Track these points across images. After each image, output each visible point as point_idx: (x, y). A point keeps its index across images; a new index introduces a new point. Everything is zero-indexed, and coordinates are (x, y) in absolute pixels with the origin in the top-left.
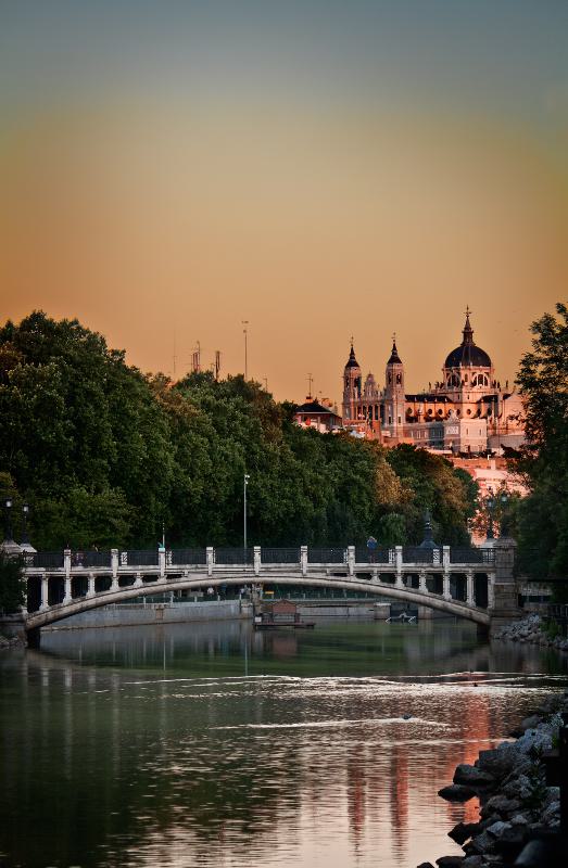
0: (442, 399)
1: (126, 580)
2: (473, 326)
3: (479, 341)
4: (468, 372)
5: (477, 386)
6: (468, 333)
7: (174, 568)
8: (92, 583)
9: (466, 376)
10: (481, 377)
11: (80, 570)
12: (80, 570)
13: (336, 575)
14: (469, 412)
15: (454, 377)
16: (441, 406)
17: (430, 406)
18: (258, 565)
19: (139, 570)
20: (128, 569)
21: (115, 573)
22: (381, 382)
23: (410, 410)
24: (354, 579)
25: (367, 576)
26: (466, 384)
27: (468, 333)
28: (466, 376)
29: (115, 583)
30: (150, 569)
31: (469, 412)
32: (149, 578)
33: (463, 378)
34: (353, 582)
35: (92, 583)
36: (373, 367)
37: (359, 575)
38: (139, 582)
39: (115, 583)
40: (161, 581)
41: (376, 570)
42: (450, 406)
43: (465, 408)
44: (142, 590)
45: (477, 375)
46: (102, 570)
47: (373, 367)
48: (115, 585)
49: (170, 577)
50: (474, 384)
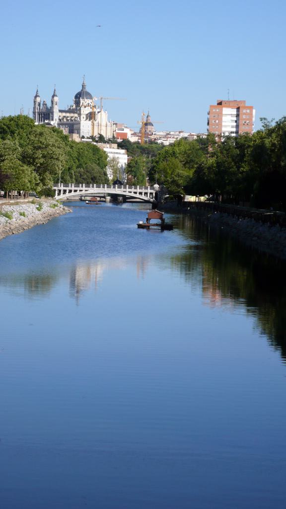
1: (75, 191)
3: (88, 89)
5: (87, 108)
6: (83, 86)
11: (65, 188)
12: (65, 188)
17: (68, 115)
18: (106, 188)
20: (76, 189)
23: (60, 116)
35: (73, 191)
37: (129, 192)
38: (78, 191)
45: (87, 103)
46: (146, 191)
49: (86, 191)
50: (85, 107)
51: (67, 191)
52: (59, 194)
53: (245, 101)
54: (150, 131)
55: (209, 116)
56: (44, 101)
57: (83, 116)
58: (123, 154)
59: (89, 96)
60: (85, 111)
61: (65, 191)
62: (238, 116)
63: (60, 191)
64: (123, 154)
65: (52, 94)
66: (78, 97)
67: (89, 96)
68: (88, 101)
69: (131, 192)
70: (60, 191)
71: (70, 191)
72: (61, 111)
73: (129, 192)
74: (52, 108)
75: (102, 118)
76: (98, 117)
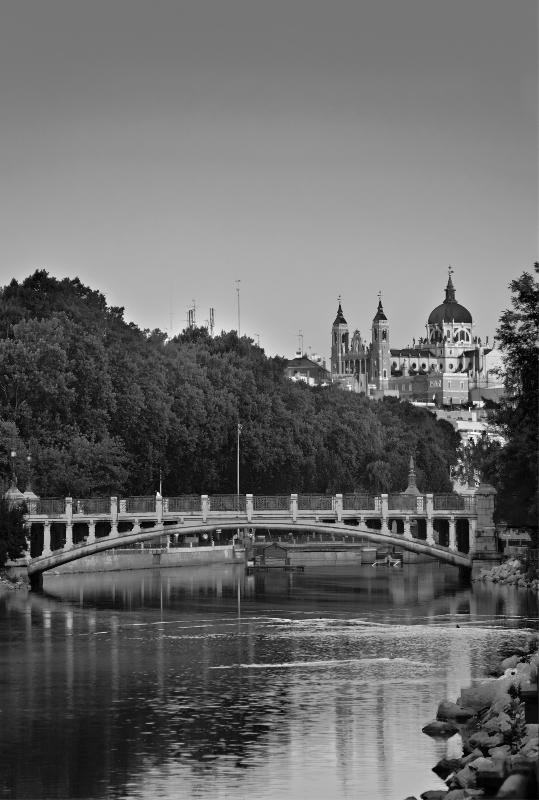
0: (426, 353)
1: (125, 526)
2: (455, 286)
3: (460, 299)
4: (449, 329)
5: (459, 342)
7: (171, 515)
8: (92, 530)
9: (448, 332)
10: (462, 333)
11: (81, 517)
12: (444, 513)
13: (325, 521)
14: (451, 366)
15: (437, 332)
19: (137, 517)
21: (69, 521)
22: (367, 339)
23: (395, 364)
24: (342, 525)
25: (354, 521)
26: (449, 339)
27: (450, 291)
28: (448, 332)
29: (114, 529)
30: (148, 516)
31: (451, 366)
32: (146, 524)
33: (445, 333)
34: (340, 528)
35: (92, 530)
36: (360, 324)
37: (348, 521)
38: (137, 528)
39: (114, 529)
40: (157, 527)
41: (137, 520)
42: (434, 361)
43: (448, 362)
44: (140, 536)
45: (458, 331)
46: (103, 516)
47: (360, 324)
48: (114, 531)
49: (166, 523)
50: (456, 340)
53: (434, 770)
56: (357, 332)
57: (451, 361)
59: (465, 317)
60: (454, 351)
63: (58, 531)
66: (435, 319)
69: (354, 521)
70: (58, 531)
72: (395, 353)
74: (374, 347)
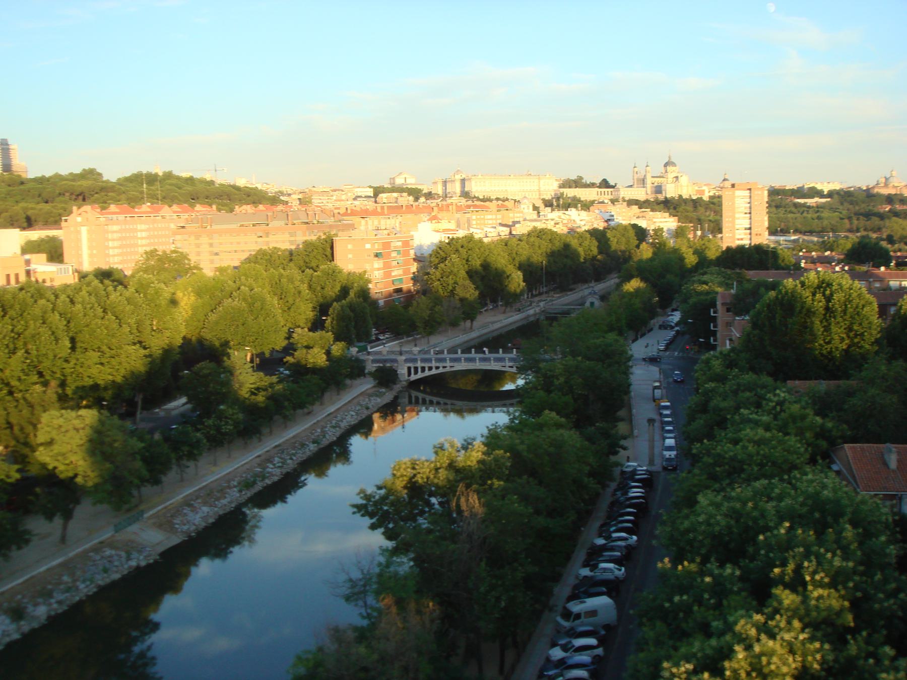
0: (663, 177)
1: (437, 368)
3: (673, 160)
6: (669, 157)
7: (452, 364)
11: (423, 365)
16: (661, 179)
17: (658, 179)
20: (438, 365)
30: (445, 365)
32: (444, 367)
37: (510, 367)
38: (441, 368)
46: (430, 365)
51: (427, 369)
52: (416, 372)
54: (142, 256)
55: (294, 200)
58: (672, 222)
59: (673, 164)
60: (671, 176)
61: (423, 369)
62: (750, 197)
64: (672, 222)
65: (646, 165)
66: (666, 165)
67: (673, 164)
68: (674, 168)
70: (416, 369)
71: (430, 369)
72: (653, 177)
73: (510, 367)
75: (684, 180)
76: (680, 179)
